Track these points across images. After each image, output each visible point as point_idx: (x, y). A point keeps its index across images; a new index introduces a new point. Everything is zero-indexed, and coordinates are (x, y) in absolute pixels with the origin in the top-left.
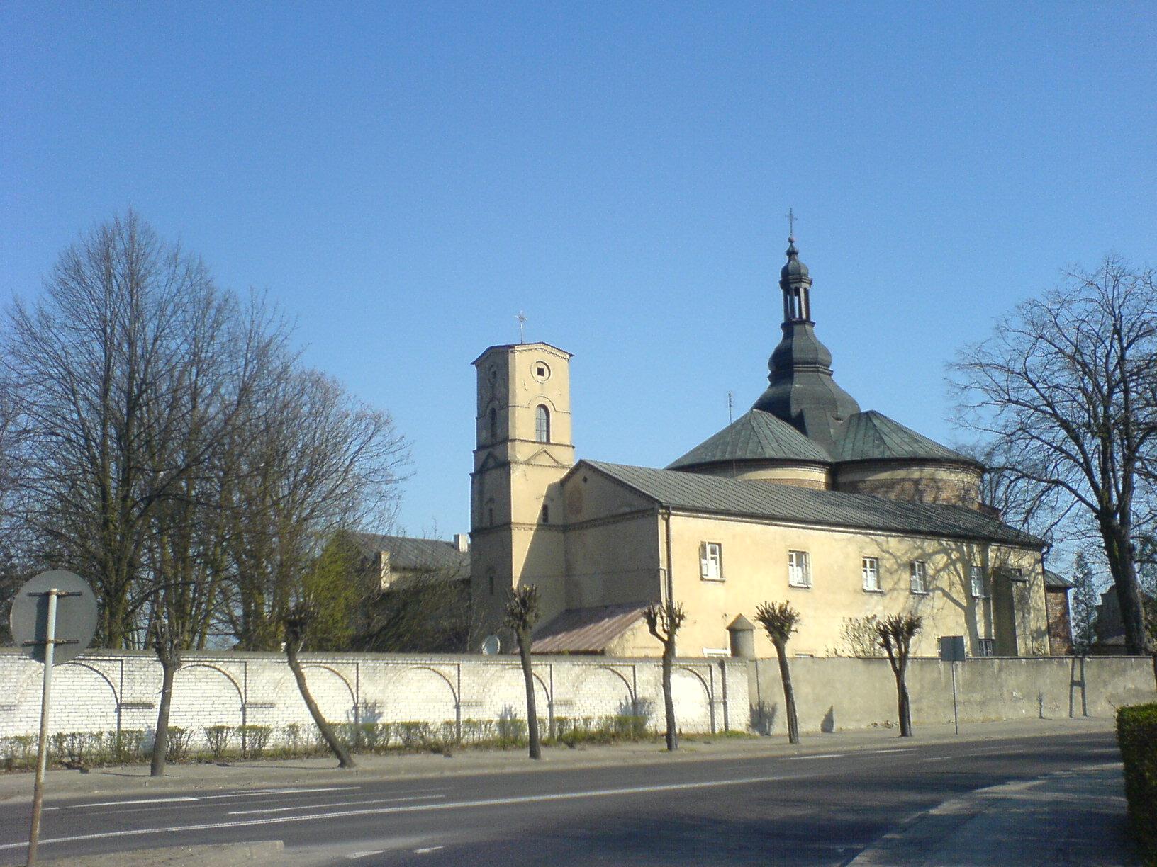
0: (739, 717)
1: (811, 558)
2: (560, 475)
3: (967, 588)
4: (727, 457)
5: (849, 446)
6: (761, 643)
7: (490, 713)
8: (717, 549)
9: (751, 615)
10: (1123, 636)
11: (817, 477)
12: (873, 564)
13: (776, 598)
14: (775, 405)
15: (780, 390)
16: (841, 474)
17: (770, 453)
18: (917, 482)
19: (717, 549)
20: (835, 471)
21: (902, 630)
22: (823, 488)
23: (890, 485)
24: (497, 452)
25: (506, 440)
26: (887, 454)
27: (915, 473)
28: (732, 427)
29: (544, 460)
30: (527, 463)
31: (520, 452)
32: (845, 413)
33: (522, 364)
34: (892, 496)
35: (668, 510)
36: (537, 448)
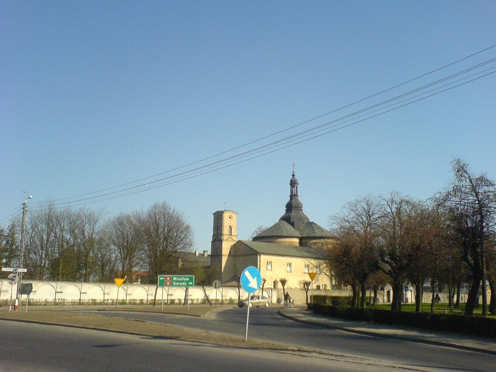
0: (274, 301)
1: (292, 265)
2: (233, 243)
3: (331, 272)
4: (273, 235)
5: (305, 232)
6: (280, 286)
7: (228, 298)
8: (271, 263)
9: (278, 280)
10: (349, 287)
11: (297, 240)
12: (308, 266)
13: (283, 277)
14: (286, 219)
15: (288, 214)
16: (303, 241)
17: (284, 234)
18: (322, 243)
19: (271, 263)
20: (301, 239)
21: (307, 284)
22: (298, 245)
23: (315, 244)
24: (219, 237)
25: (221, 234)
26: (315, 235)
27: (322, 241)
28: (275, 225)
29: (230, 239)
30: (226, 240)
31: (225, 238)
32: (305, 222)
33: (226, 216)
34: (316, 247)
35: (260, 254)
36: (229, 236)
